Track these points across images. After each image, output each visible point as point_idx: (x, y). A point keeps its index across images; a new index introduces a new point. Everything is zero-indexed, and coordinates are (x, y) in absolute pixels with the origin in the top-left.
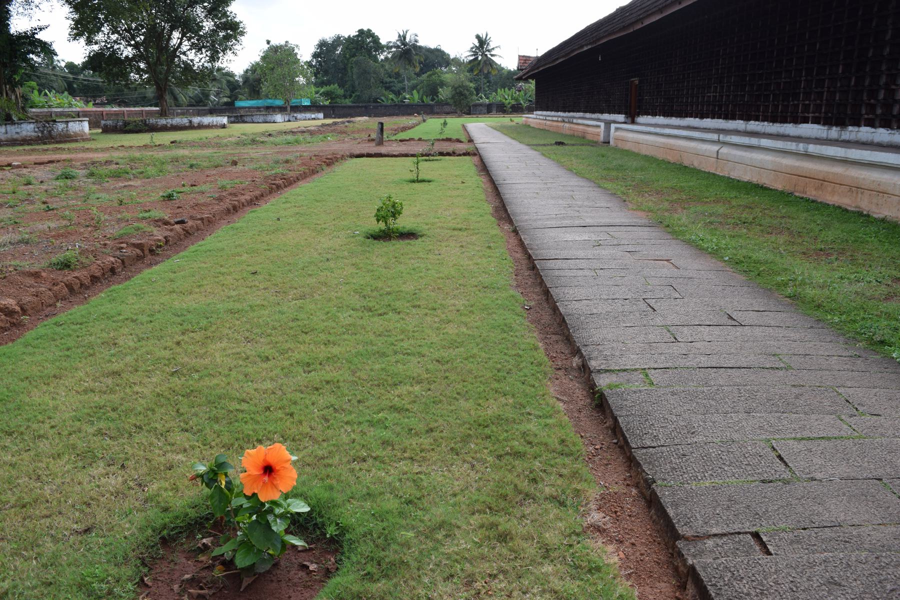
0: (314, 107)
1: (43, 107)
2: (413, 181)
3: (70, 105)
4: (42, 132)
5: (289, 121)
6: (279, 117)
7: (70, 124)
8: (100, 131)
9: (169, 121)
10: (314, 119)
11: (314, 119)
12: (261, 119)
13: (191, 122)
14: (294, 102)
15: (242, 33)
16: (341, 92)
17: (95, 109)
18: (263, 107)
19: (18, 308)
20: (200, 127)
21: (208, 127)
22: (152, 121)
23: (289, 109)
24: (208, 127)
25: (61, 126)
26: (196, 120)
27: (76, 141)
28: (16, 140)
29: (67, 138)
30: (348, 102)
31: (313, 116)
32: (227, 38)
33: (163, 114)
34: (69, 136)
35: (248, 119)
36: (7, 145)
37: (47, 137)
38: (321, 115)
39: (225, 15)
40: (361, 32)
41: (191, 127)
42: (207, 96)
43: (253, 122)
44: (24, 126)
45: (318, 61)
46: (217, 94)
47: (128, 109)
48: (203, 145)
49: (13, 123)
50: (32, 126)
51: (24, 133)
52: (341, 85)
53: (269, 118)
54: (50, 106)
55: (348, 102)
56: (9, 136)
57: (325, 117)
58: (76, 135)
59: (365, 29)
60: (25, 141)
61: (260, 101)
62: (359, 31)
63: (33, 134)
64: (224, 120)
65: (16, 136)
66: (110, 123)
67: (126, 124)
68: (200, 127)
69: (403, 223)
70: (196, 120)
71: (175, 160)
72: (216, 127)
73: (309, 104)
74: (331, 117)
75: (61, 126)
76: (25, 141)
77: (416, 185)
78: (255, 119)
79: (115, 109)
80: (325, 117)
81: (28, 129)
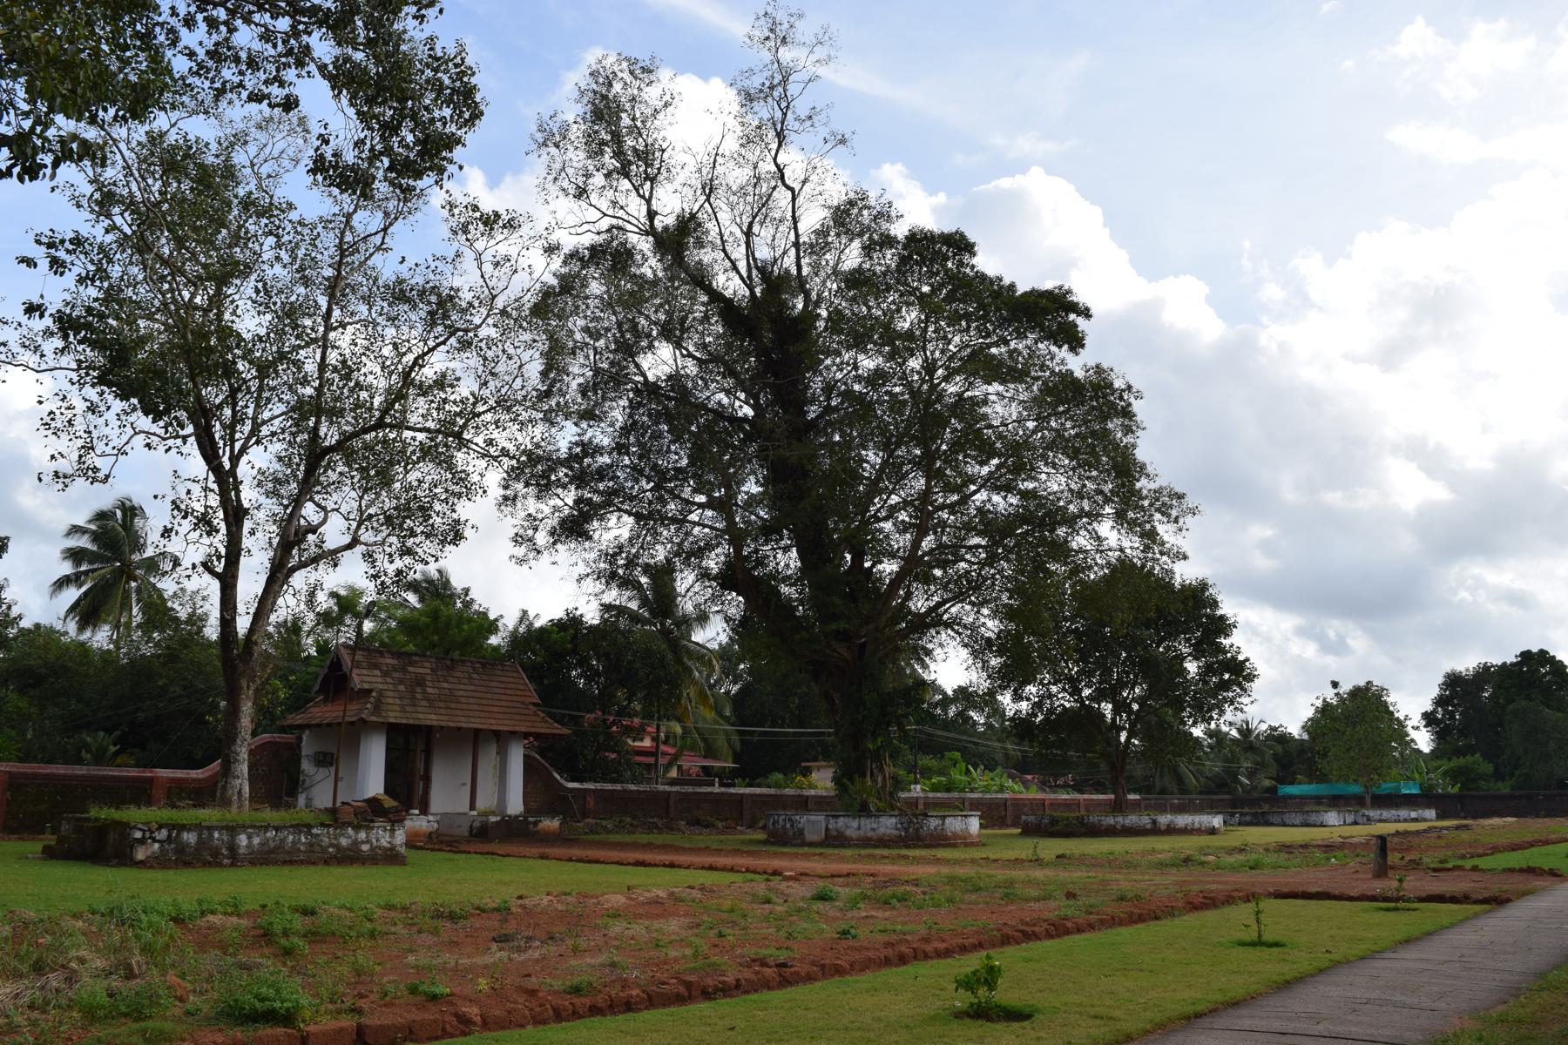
0: (1426, 798)
1: (963, 791)
2: (1253, 944)
3: (1002, 789)
4: (906, 830)
5: (1355, 823)
6: (1332, 817)
7: (948, 821)
8: (761, 836)
9: (1120, 819)
10: (1415, 820)
11: (1415, 820)
12: (1298, 819)
13: (1154, 822)
14: (1386, 787)
15: (1251, 678)
16: (1488, 768)
17: (1041, 796)
18: (1326, 797)
19: (478, 1019)
20: (1171, 831)
21: (1185, 831)
22: (1093, 819)
23: (1368, 801)
24: (1185, 831)
25: (933, 823)
26: (1164, 819)
27: (955, 846)
28: (869, 839)
29: (941, 840)
30: (1504, 788)
31: (1414, 814)
32: (1225, 685)
33: (1118, 807)
34: (946, 838)
35: (1276, 819)
36: (857, 846)
37: (913, 838)
38: (1431, 813)
39: (1221, 650)
40: (1526, 656)
41: (1155, 831)
42: (1234, 776)
43: (1285, 825)
44: (883, 820)
45: (1446, 712)
46: (1251, 774)
47: (1052, 796)
48: (1112, 863)
49: (869, 815)
50: (893, 820)
51: (882, 830)
52: (1487, 757)
53: (1313, 818)
54: (972, 791)
55: (1504, 788)
56: (862, 833)
57: (1440, 817)
58: (955, 836)
59: (1535, 650)
60: (883, 842)
61: (1322, 786)
62: (1523, 654)
63: (895, 832)
64: (1217, 821)
65: (870, 834)
66: (1031, 819)
67: (1054, 821)
68: (1171, 831)
69: (1005, 994)
70: (1164, 819)
71: (952, 880)
72: (1199, 831)
73: (1415, 791)
74: (1456, 816)
75: (933, 823)
76: (883, 842)
77: (1258, 952)
78: (1288, 818)
79: (1066, 797)
80: (1440, 817)
81: (887, 825)
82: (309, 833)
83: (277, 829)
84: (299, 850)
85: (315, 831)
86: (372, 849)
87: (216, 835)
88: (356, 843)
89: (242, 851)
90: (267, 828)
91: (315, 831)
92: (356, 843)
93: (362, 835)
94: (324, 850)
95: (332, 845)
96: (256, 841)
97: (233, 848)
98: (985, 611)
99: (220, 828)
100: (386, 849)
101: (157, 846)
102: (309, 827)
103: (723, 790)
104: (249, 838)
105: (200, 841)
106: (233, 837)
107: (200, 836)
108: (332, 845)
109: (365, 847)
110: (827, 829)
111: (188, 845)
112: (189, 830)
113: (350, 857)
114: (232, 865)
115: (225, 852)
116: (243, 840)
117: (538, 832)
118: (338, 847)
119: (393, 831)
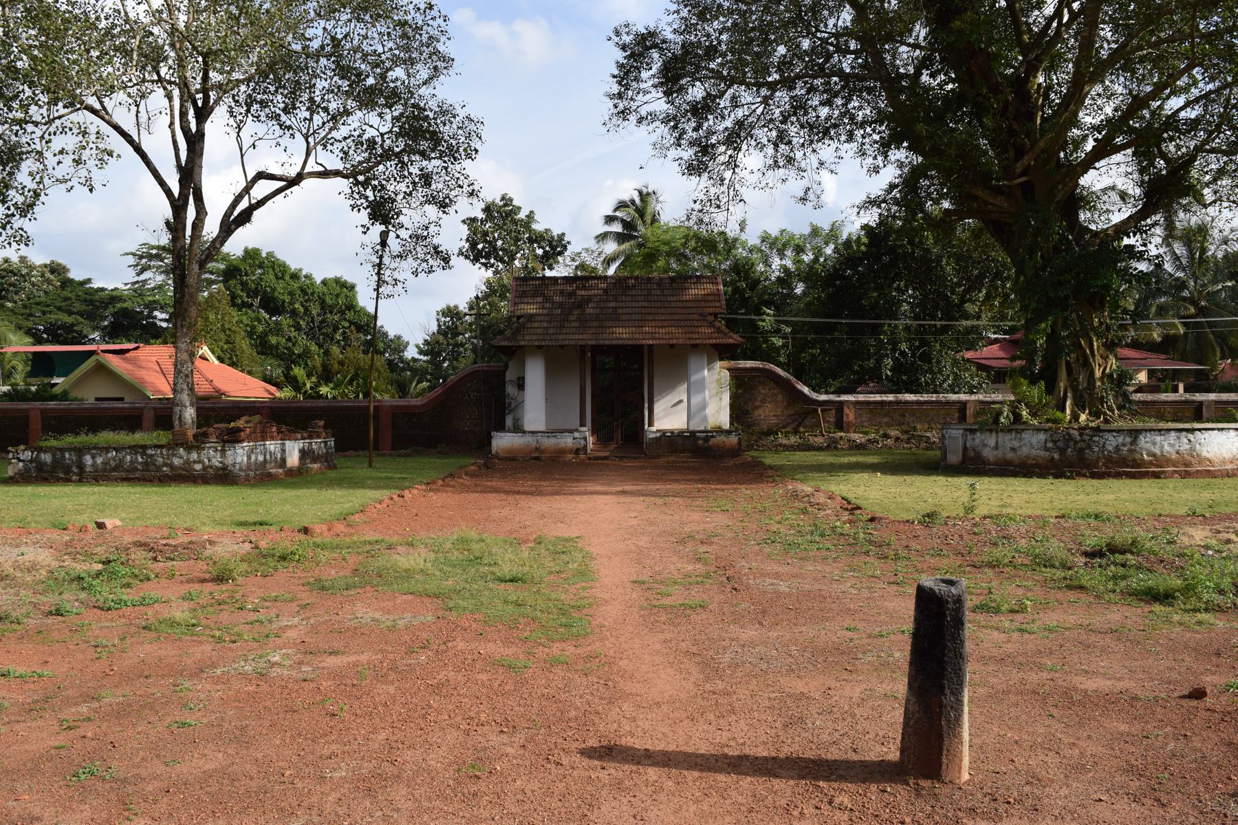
4: (1062, 451)
28: (1008, 463)
34: (1137, 463)
56: (999, 453)
63: (1042, 453)
65: (1010, 456)
82: (143, 454)
83: (116, 449)
84: (136, 469)
85: (149, 452)
86: (204, 468)
87: (67, 456)
88: (187, 462)
89: (88, 469)
90: (107, 449)
91: (149, 452)
92: (187, 462)
93: (194, 456)
94: (158, 469)
95: (166, 465)
96: (99, 460)
97: (81, 466)
98: (371, 81)
99: (70, 450)
100: (218, 469)
101: (21, 464)
102: (145, 447)
103: (1188, 396)
104: (93, 458)
105: (55, 460)
106: (80, 457)
107: (54, 456)
108: (166, 465)
109: (198, 467)
110: (965, 449)
111: (45, 464)
112: (45, 452)
113: (185, 477)
114: (80, 481)
115: (75, 469)
116: (88, 460)
117: (710, 448)
118: (171, 466)
119: (223, 451)
